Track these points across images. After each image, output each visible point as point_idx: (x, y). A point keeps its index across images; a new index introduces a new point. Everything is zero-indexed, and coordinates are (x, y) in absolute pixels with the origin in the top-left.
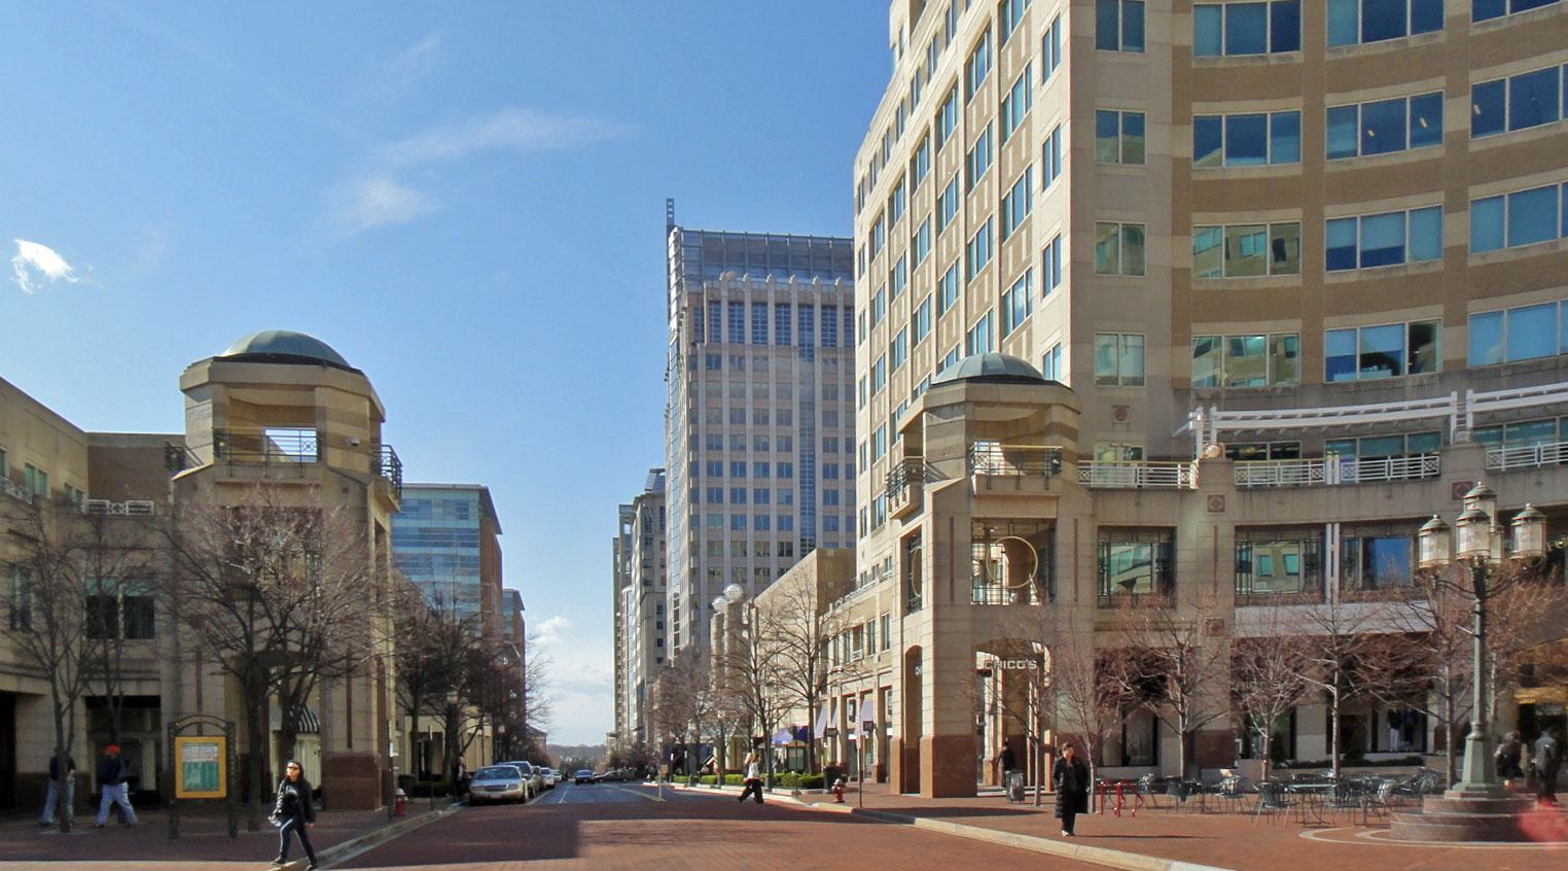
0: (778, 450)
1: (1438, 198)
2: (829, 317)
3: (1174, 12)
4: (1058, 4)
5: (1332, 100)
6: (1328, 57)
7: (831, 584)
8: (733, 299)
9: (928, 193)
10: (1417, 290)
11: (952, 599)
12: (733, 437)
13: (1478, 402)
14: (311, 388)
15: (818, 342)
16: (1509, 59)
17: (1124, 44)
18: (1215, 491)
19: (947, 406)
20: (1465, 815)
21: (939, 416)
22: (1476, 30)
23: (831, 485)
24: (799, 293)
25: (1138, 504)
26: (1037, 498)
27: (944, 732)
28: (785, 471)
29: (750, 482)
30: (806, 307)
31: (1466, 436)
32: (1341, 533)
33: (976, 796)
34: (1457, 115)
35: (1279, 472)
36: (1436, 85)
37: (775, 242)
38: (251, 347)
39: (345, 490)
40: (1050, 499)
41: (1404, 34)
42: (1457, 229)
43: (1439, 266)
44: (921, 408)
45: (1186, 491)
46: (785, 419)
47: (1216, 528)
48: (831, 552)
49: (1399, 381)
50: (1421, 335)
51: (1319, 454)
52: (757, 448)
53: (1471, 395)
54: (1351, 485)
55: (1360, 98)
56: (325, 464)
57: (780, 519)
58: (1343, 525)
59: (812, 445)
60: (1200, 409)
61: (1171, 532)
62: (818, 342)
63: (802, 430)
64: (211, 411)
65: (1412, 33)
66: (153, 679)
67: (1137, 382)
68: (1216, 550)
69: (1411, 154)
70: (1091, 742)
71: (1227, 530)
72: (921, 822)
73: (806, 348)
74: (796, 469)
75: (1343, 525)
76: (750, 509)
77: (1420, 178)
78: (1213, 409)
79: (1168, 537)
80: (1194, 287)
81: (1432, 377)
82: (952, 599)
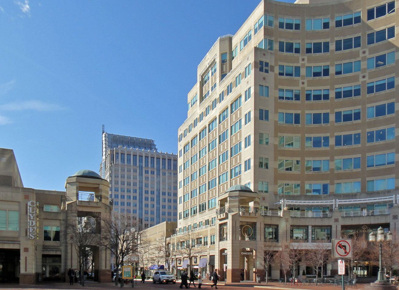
0: (133, 193)
1: (328, 158)
2: (147, 161)
3: (275, 113)
4: (250, 109)
5: (307, 135)
6: (306, 126)
7: (169, 230)
8: (122, 153)
9: (206, 141)
10: (323, 177)
11: (236, 239)
12: (121, 189)
13: (339, 202)
14: (99, 184)
15: (144, 166)
16: (342, 131)
17: (265, 119)
18: (287, 217)
19: (234, 196)
20: (380, 286)
21: (232, 198)
22: (336, 124)
23: (147, 202)
24: (145, 154)
25: (271, 219)
26: (253, 217)
27: (233, 268)
28: (135, 198)
29: (126, 200)
30: (141, 156)
31: (337, 209)
32: (312, 228)
33: (240, 282)
34: (332, 141)
35: (298, 214)
36: (328, 135)
37: (132, 139)
38: (83, 174)
39: (106, 208)
40: (256, 218)
41: (321, 123)
42: (332, 165)
43: (329, 172)
44: (228, 196)
45: (280, 217)
46: (135, 184)
47: (287, 225)
48: (169, 222)
49: (321, 196)
50: (325, 187)
51: (304, 210)
52: (128, 191)
53: (337, 200)
54: (314, 218)
55: (312, 136)
56: (102, 202)
57: (133, 210)
58: (312, 226)
59: (142, 192)
60: (282, 199)
61: (277, 226)
62: (144, 166)
63: (139, 188)
64: (76, 188)
65: (323, 123)
66: (60, 251)
67: (266, 192)
68: (286, 231)
69: (323, 148)
70: (286, 271)
71: (289, 226)
72: (255, 287)
73: (141, 167)
74: (138, 198)
75: (312, 226)
76: (126, 207)
77: (325, 154)
78: (285, 200)
79: (277, 227)
80: (279, 172)
81: (327, 195)
82: (236, 239)
